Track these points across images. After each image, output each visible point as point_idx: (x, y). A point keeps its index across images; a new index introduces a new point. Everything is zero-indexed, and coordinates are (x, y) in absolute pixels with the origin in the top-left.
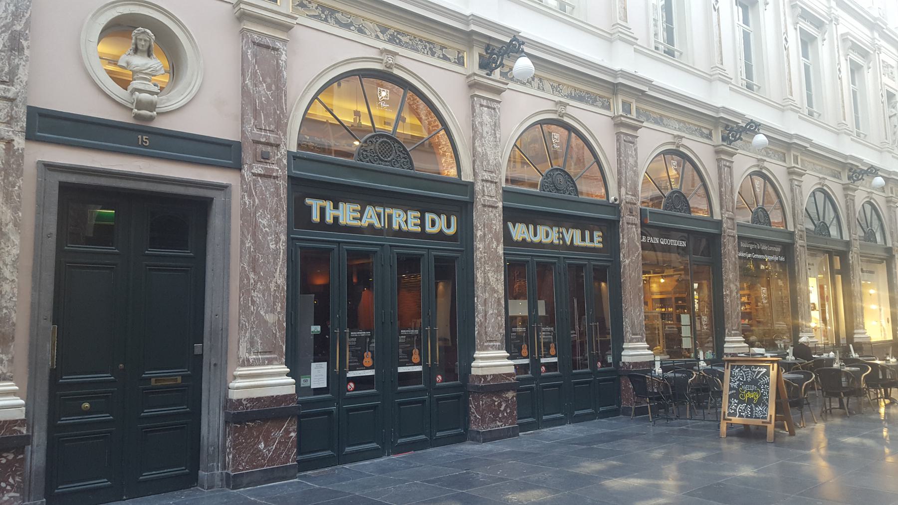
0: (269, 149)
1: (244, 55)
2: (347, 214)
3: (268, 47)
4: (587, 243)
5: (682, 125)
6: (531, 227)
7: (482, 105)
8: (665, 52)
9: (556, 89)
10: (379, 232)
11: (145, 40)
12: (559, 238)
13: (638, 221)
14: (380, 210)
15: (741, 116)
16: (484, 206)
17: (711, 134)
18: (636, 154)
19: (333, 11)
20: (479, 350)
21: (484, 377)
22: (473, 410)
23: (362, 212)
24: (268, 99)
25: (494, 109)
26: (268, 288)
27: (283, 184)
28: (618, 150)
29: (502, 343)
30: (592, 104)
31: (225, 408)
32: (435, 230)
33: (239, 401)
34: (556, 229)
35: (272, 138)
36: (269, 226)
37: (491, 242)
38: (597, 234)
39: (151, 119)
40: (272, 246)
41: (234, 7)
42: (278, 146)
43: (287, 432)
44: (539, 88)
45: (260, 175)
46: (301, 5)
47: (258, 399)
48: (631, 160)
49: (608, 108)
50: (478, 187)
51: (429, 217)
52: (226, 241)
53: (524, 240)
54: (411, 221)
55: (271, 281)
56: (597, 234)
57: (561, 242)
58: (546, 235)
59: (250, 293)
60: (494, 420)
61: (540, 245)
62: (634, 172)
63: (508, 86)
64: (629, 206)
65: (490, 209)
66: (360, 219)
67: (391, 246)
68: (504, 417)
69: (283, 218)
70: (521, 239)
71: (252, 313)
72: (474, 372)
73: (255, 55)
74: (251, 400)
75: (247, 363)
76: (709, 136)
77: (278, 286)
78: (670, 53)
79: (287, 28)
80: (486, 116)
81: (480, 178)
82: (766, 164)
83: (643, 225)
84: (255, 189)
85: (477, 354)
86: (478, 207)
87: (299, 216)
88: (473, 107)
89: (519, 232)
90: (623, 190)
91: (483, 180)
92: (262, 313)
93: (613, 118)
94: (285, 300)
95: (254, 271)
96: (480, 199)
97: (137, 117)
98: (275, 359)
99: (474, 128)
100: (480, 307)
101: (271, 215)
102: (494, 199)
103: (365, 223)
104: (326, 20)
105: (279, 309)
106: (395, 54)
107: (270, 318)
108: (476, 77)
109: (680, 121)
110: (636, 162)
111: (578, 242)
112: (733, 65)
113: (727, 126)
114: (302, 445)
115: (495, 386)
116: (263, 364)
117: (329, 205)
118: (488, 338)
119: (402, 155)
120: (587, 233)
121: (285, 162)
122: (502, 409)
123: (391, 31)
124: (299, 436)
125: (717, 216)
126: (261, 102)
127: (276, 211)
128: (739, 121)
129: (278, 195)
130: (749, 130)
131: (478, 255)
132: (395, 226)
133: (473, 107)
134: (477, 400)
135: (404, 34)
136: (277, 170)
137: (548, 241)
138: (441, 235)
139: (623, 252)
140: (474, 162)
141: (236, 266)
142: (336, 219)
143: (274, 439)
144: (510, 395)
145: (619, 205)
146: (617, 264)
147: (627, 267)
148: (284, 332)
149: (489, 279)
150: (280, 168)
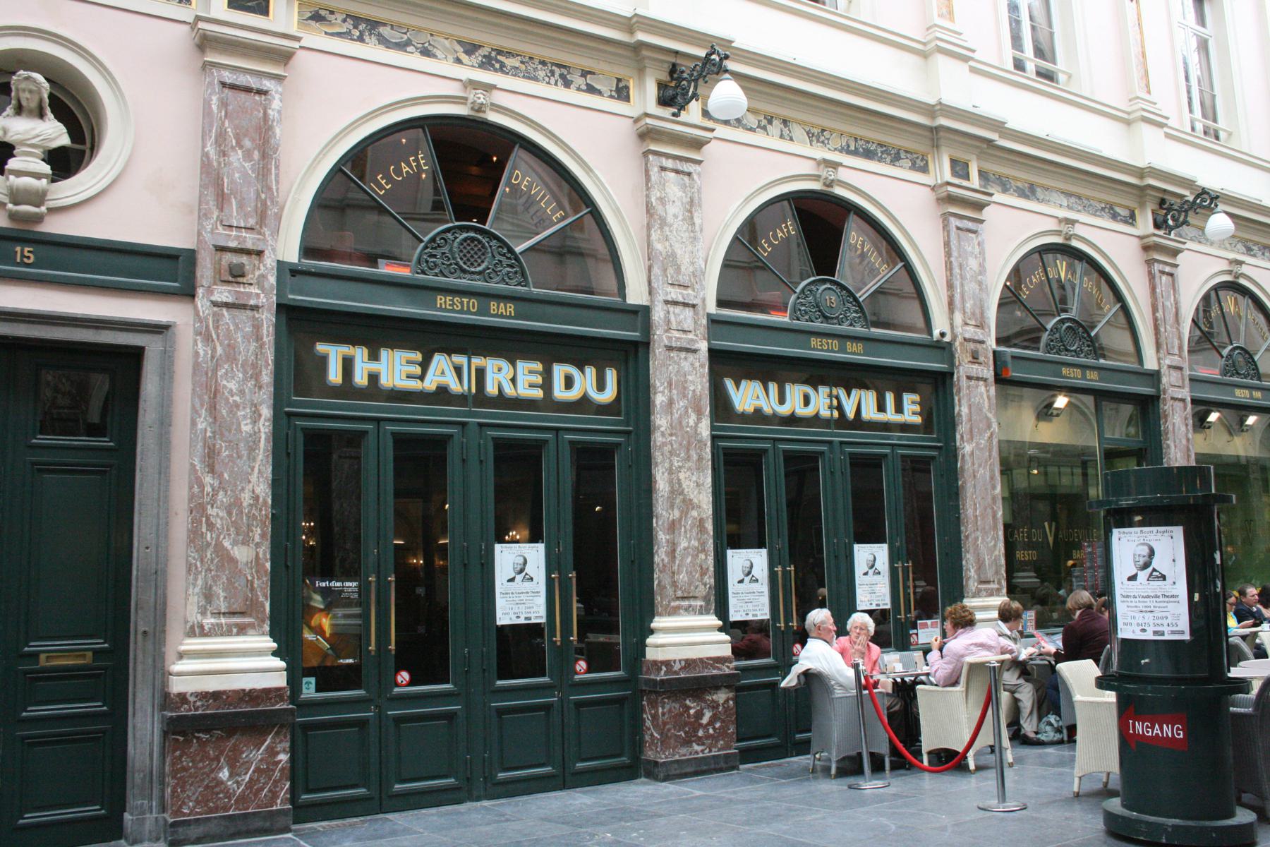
0: (244, 259)
1: (207, 103)
2: (395, 368)
3: (248, 90)
4: (890, 416)
5: (1073, 200)
6: (773, 387)
7: (663, 169)
8: (1039, 74)
9: (819, 135)
11: (31, 91)
12: (831, 407)
13: (989, 373)
14: (461, 360)
15: (1188, 183)
16: (670, 348)
17: (1133, 216)
18: (982, 253)
19: (373, 24)
20: (661, 615)
21: (667, 663)
22: (648, 724)
23: (425, 365)
24: (245, 175)
25: (689, 174)
26: (237, 503)
27: (268, 319)
28: (947, 244)
29: (706, 599)
30: (892, 163)
31: (163, 707)
32: (574, 394)
33: (183, 697)
34: (824, 390)
35: (250, 240)
36: (242, 392)
38: (908, 398)
39: (39, 219)
40: (246, 428)
41: (193, 29)
42: (260, 253)
43: (272, 752)
44: (782, 137)
45: (226, 305)
46: (317, 17)
47: (216, 695)
48: (973, 263)
49: (924, 169)
50: (658, 315)
52: (165, 422)
53: (758, 411)
55: (243, 489)
56: (908, 398)
57: (836, 414)
58: (799, 400)
59: (204, 509)
60: (687, 742)
61: (792, 420)
62: (980, 284)
63: (715, 134)
64: (971, 346)
65: (683, 355)
66: (422, 378)
67: (481, 425)
68: (708, 736)
69: (267, 377)
70: (752, 410)
71: (209, 545)
72: (651, 654)
73: (224, 104)
74: (204, 696)
75: (197, 631)
76: (1131, 219)
77: (256, 498)
78: (1048, 76)
79: (284, 57)
80: (673, 187)
82: (1244, 269)
83: (1000, 380)
84: (217, 328)
85: (657, 623)
86: (658, 353)
87: (296, 373)
88: (647, 171)
89: (747, 396)
90: (958, 318)
91: (667, 302)
92: (227, 544)
93: (933, 188)
94: (268, 523)
95: (212, 470)
96: (660, 337)
97: (13, 216)
98: (251, 626)
99: (649, 209)
100: (662, 536)
101: (245, 372)
102: (691, 336)
103: (430, 384)
104: (361, 39)
105: (257, 539)
106: (489, 88)
107: (242, 554)
108: (649, 121)
109: (1068, 194)
110: (982, 266)
111: (870, 412)
112: (1169, 98)
113: (1162, 202)
114: (300, 775)
116: (229, 633)
117: (360, 354)
118: (679, 594)
119: (505, 262)
120: (890, 398)
121: (272, 279)
122: (705, 720)
123: (484, 51)
124: (292, 760)
125: (1150, 363)
126: (232, 182)
127: (254, 366)
128: (1186, 193)
129: (258, 338)
130: (1201, 206)
131: (657, 439)
132: (491, 389)
133: (647, 171)
134: (654, 705)
135: (509, 54)
136: (258, 295)
137: (808, 412)
138: (584, 403)
139: (962, 429)
140: (650, 269)
141: (184, 457)
142: (374, 378)
143: (249, 763)
144: (721, 696)
145: (950, 344)
146: (950, 453)
147: (967, 458)
148: (266, 579)
149: (683, 485)
150: (262, 291)
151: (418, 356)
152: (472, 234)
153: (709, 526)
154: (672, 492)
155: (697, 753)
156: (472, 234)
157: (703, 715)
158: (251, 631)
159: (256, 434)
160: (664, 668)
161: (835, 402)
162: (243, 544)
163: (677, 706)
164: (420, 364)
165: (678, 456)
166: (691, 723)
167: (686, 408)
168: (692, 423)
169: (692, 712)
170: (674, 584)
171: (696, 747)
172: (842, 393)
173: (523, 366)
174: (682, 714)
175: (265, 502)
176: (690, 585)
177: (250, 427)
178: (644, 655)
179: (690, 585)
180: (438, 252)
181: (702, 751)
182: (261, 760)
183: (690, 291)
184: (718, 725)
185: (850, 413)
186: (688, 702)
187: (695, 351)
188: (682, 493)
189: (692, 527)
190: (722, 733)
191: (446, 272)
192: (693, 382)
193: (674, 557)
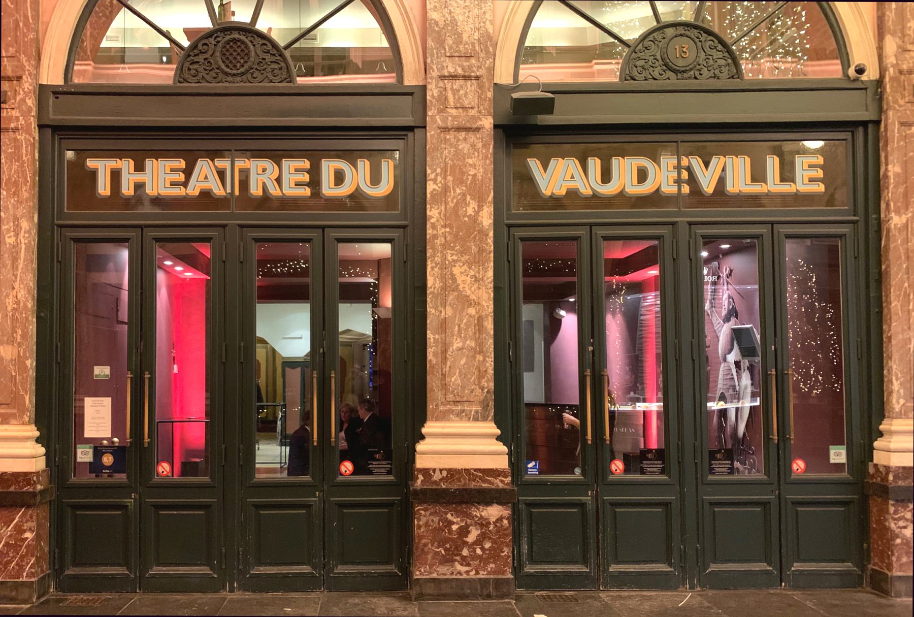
4: (773, 184)
10: (222, 202)
12: (678, 182)
16: (446, 130)
23: (188, 172)
29: (485, 407)
32: (345, 190)
37: (462, 202)
43: (19, 530)
50: (433, 92)
51: (328, 167)
54: (290, 178)
55: (8, 295)
57: (686, 189)
60: (448, 560)
66: (185, 184)
68: (474, 557)
72: (421, 463)
81: (435, 73)
91: (442, 78)
98: (13, 416)
102: (473, 112)
103: (194, 189)
115: (463, 492)
117: (126, 165)
118: (450, 397)
119: (268, 57)
122: (471, 538)
127: (16, 183)
132: (255, 190)
137: (646, 188)
138: (357, 197)
142: (139, 186)
144: (494, 512)
151: (182, 164)
152: (236, 35)
153: (489, 325)
154: (444, 288)
155: (460, 573)
156: (236, 35)
157: (469, 532)
158: (13, 421)
159: (16, 246)
160: (421, 477)
161: (685, 175)
162: (7, 343)
163: (436, 519)
164: (184, 171)
165: (453, 249)
166: (453, 540)
167: (464, 195)
168: (470, 211)
169: (455, 527)
170: (445, 386)
171: (459, 567)
172: (696, 163)
173: (289, 165)
174: (441, 529)
175: (25, 306)
176: (463, 387)
177: (13, 239)
178: (414, 461)
179: (463, 387)
180: (201, 58)
181: (467, 572)
182: (10, 536)
183: (473, 61)
184: (487, 545)
185: (708, 184)
186: (449, 516)
187: (478, 129)
188: (456, 289)
189: (468, 325)
190: (494, 555)
191: (208, 77)
192: (474, 166)
193: (445, 359)
